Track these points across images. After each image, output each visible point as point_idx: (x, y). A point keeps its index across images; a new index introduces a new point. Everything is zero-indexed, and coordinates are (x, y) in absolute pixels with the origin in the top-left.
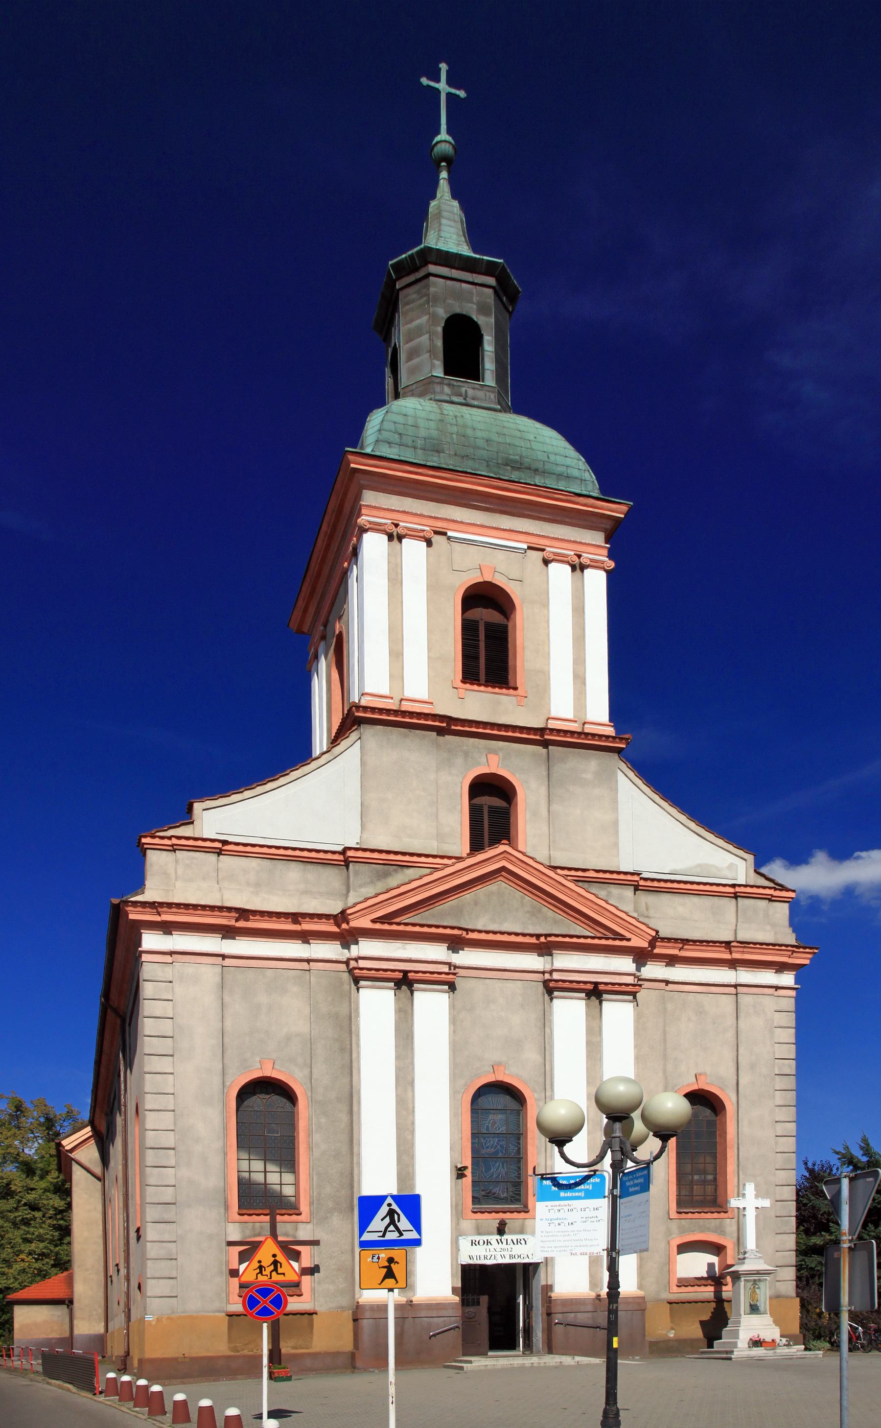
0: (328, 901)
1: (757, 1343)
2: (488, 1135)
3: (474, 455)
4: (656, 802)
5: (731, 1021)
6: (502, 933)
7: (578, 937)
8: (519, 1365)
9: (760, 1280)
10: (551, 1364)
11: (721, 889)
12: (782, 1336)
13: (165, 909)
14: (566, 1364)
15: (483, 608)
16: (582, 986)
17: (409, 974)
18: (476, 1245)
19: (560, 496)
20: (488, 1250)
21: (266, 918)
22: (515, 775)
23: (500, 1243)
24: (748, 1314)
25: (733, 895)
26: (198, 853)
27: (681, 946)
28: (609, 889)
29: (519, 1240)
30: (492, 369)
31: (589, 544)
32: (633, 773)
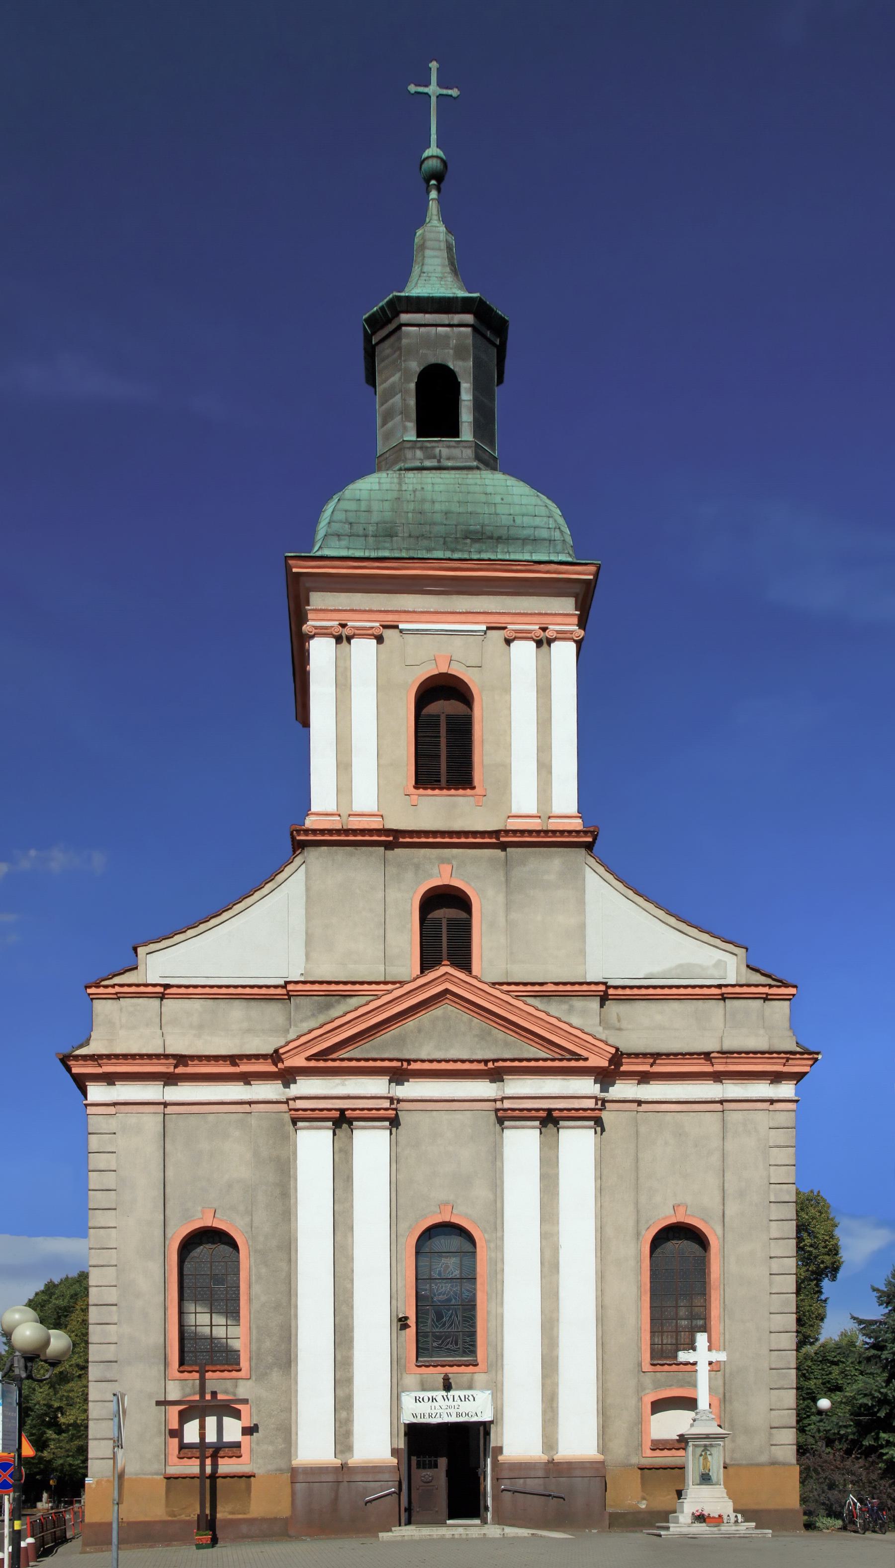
0: (270, 1039)
1: (700, 1518)
2: (440, 1281)
3: (430, 533)
4: (629, 898)
5: (716, 1143)
6: (447, 1061)
7: (537, 1060)
9: (711, 1446)
10: (474, 1536)
11: (706, 991)
12: (735, 1511)
13: (105, 1061)
14: (490, 1536)
15: (445, 700)
16: (534, 1113)
18: (420, 1402)
19: (519, 567)
20: (433, 1408)
21: (205, 1062)
22: (469, 884)
23: (446, 1400)
24: (698, 1485)
25: (720, 997)
26: (141, 999)
27: (651, 1061)
28: (571, 1002)
29: (467, 1397)
30: (469, 421)
31: (555, 614)
32: (603, 868)
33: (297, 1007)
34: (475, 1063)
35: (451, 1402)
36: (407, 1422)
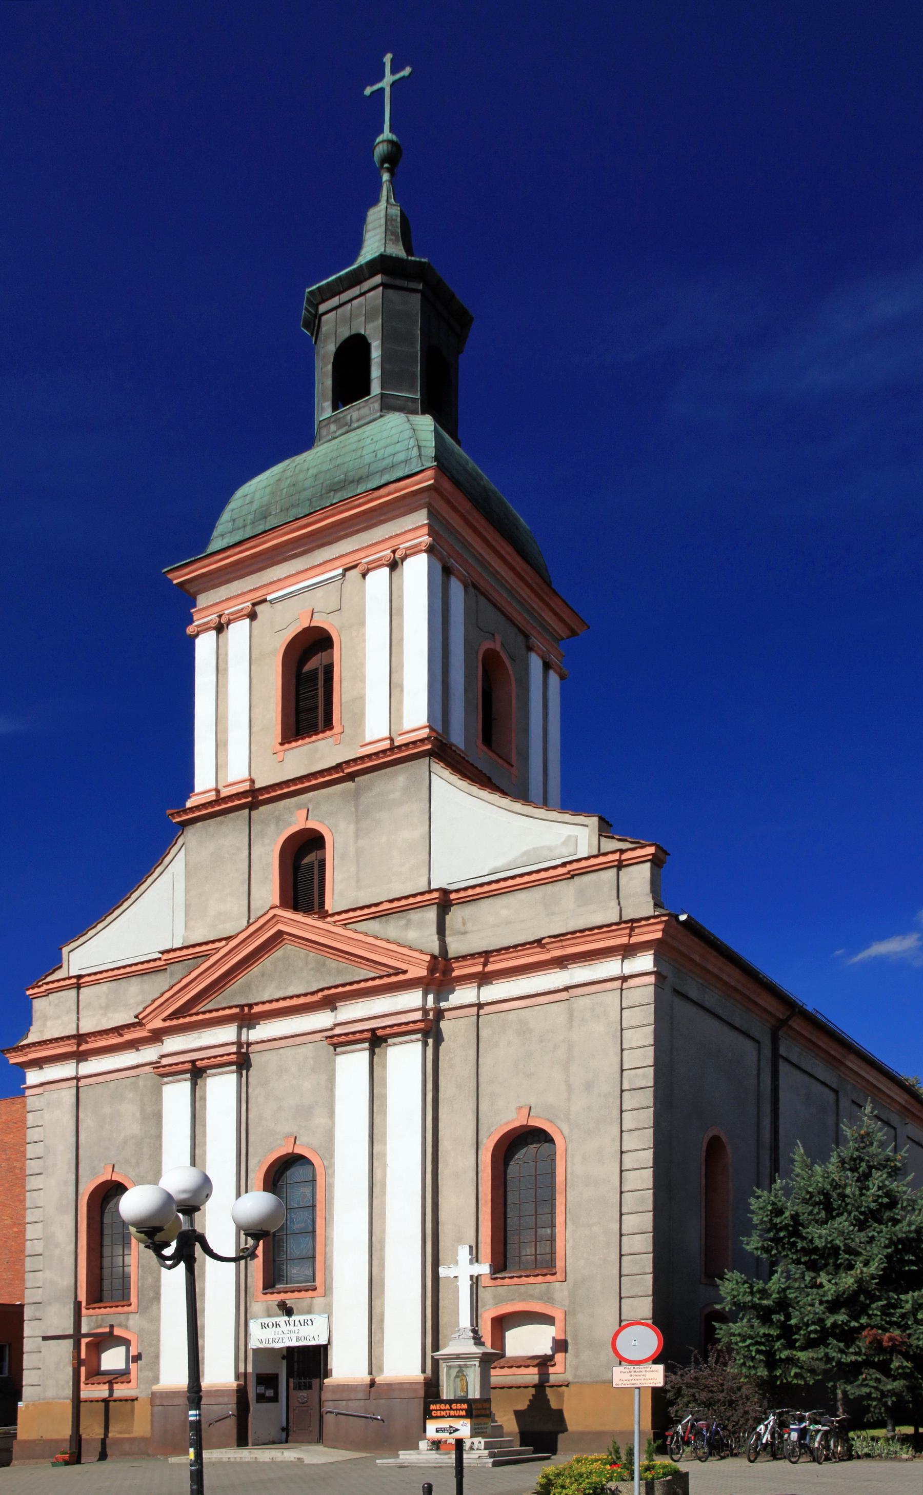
7: (366, 980)
8: (217, 1460)
9: (466, 1366)
15: (322, 652)
16: (358, 1036)
17: (197, 1063)
19: (361, 501)
23: (288, 1325)
27: (482, 960)
28: (408, 917)
29: (306, 1321)
31: (406, 532)
33: (172, 974)
34: (309, 996)
35: (292, 1328)
36: (254, 1347)
